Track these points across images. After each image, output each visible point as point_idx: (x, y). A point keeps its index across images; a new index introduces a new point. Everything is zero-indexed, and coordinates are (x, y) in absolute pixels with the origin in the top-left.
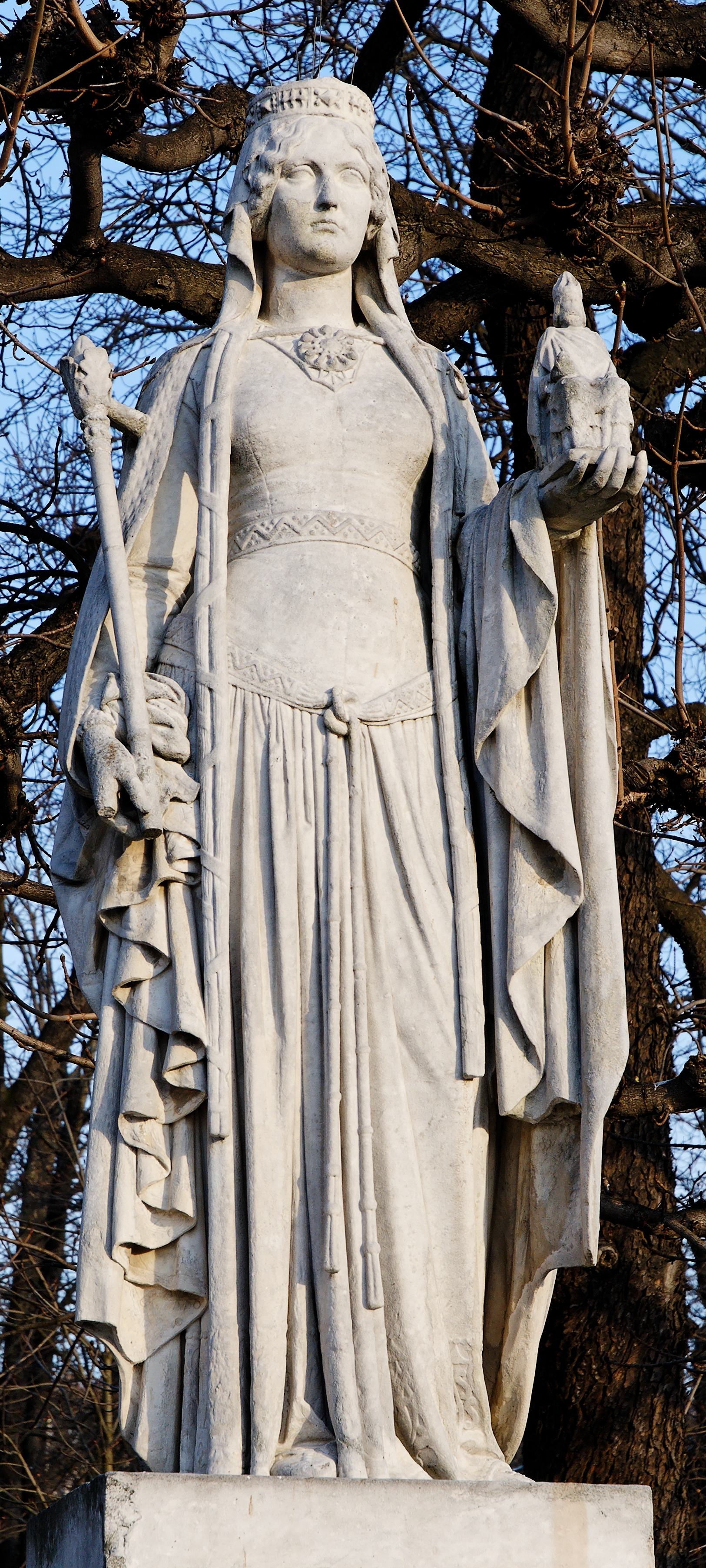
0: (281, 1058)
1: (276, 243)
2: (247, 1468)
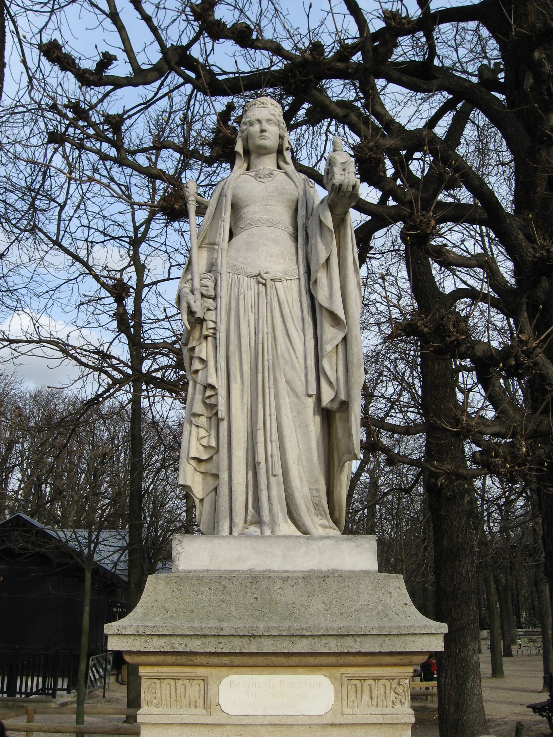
0: (242, 391)
1: (251, 146)
2: (231, 533)
